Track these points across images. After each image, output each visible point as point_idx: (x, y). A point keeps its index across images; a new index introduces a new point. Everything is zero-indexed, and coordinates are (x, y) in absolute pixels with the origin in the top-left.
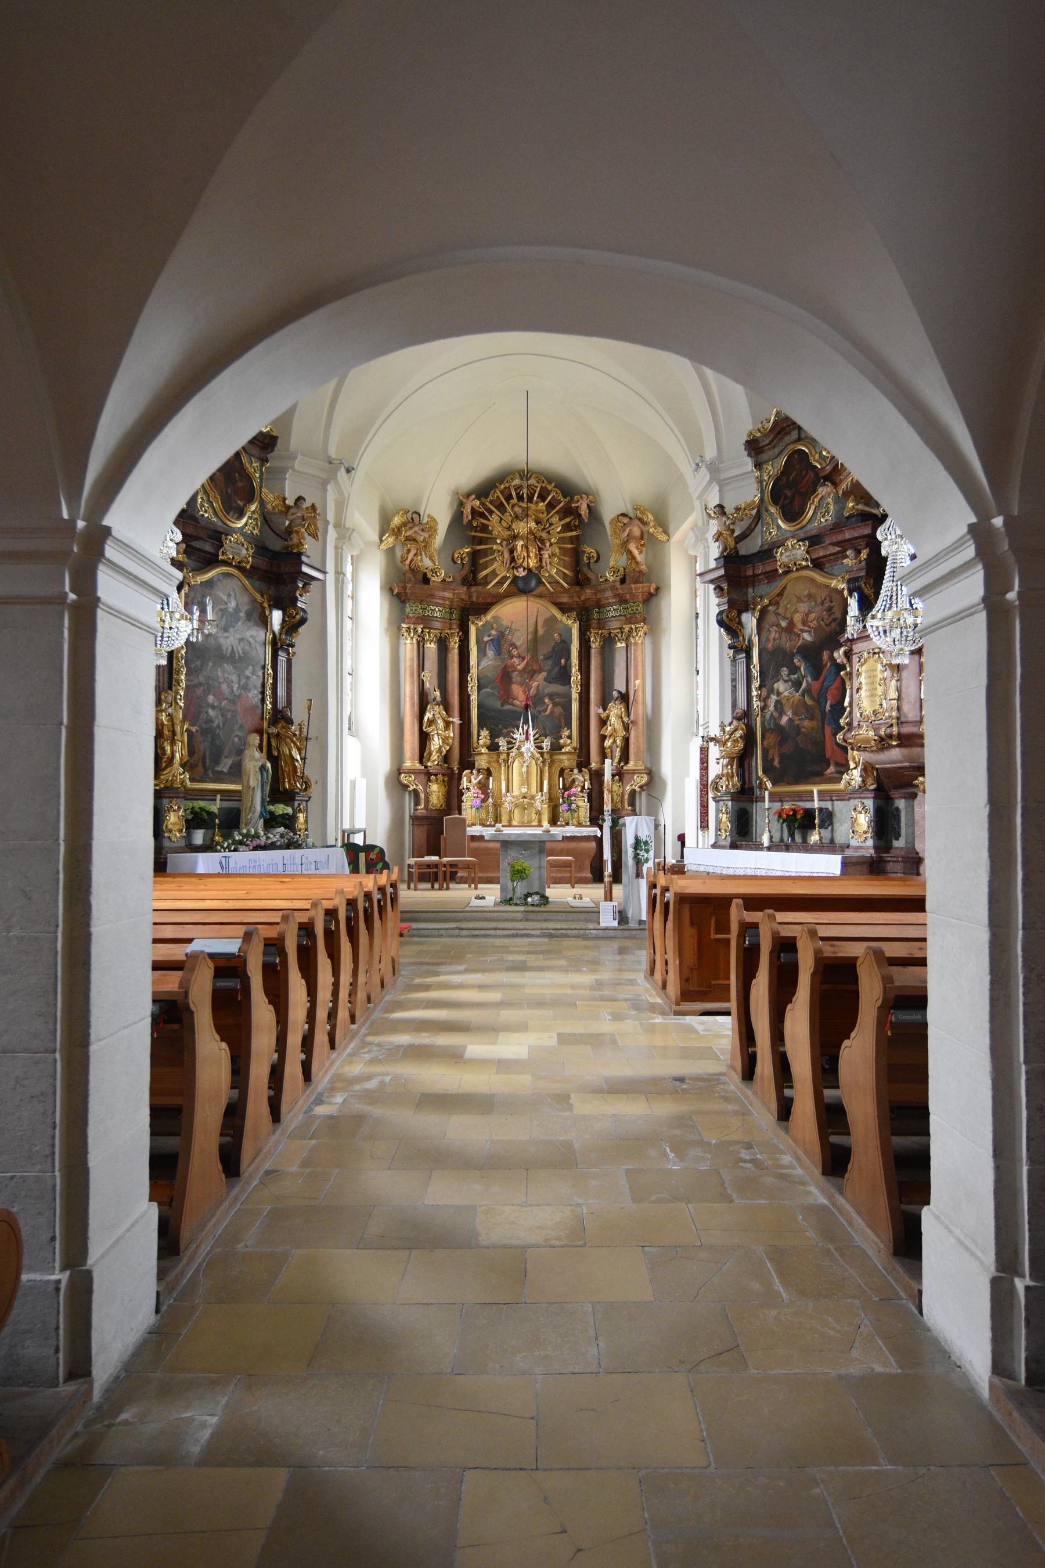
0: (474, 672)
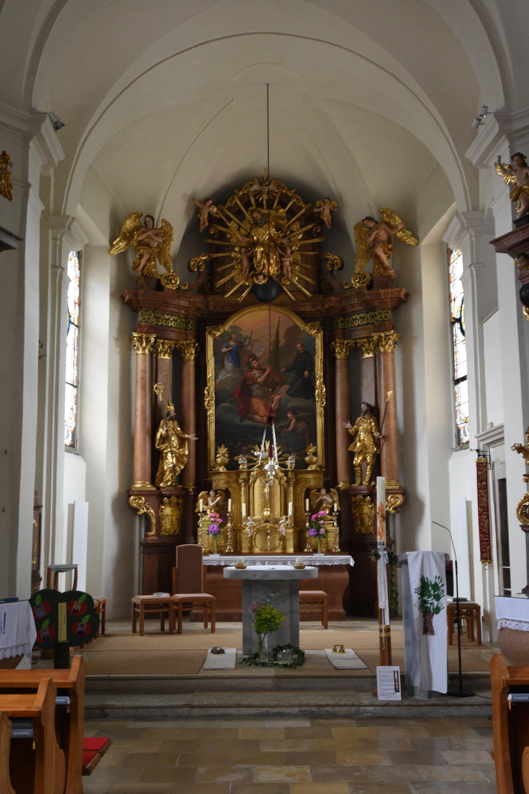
0: (211, 385)
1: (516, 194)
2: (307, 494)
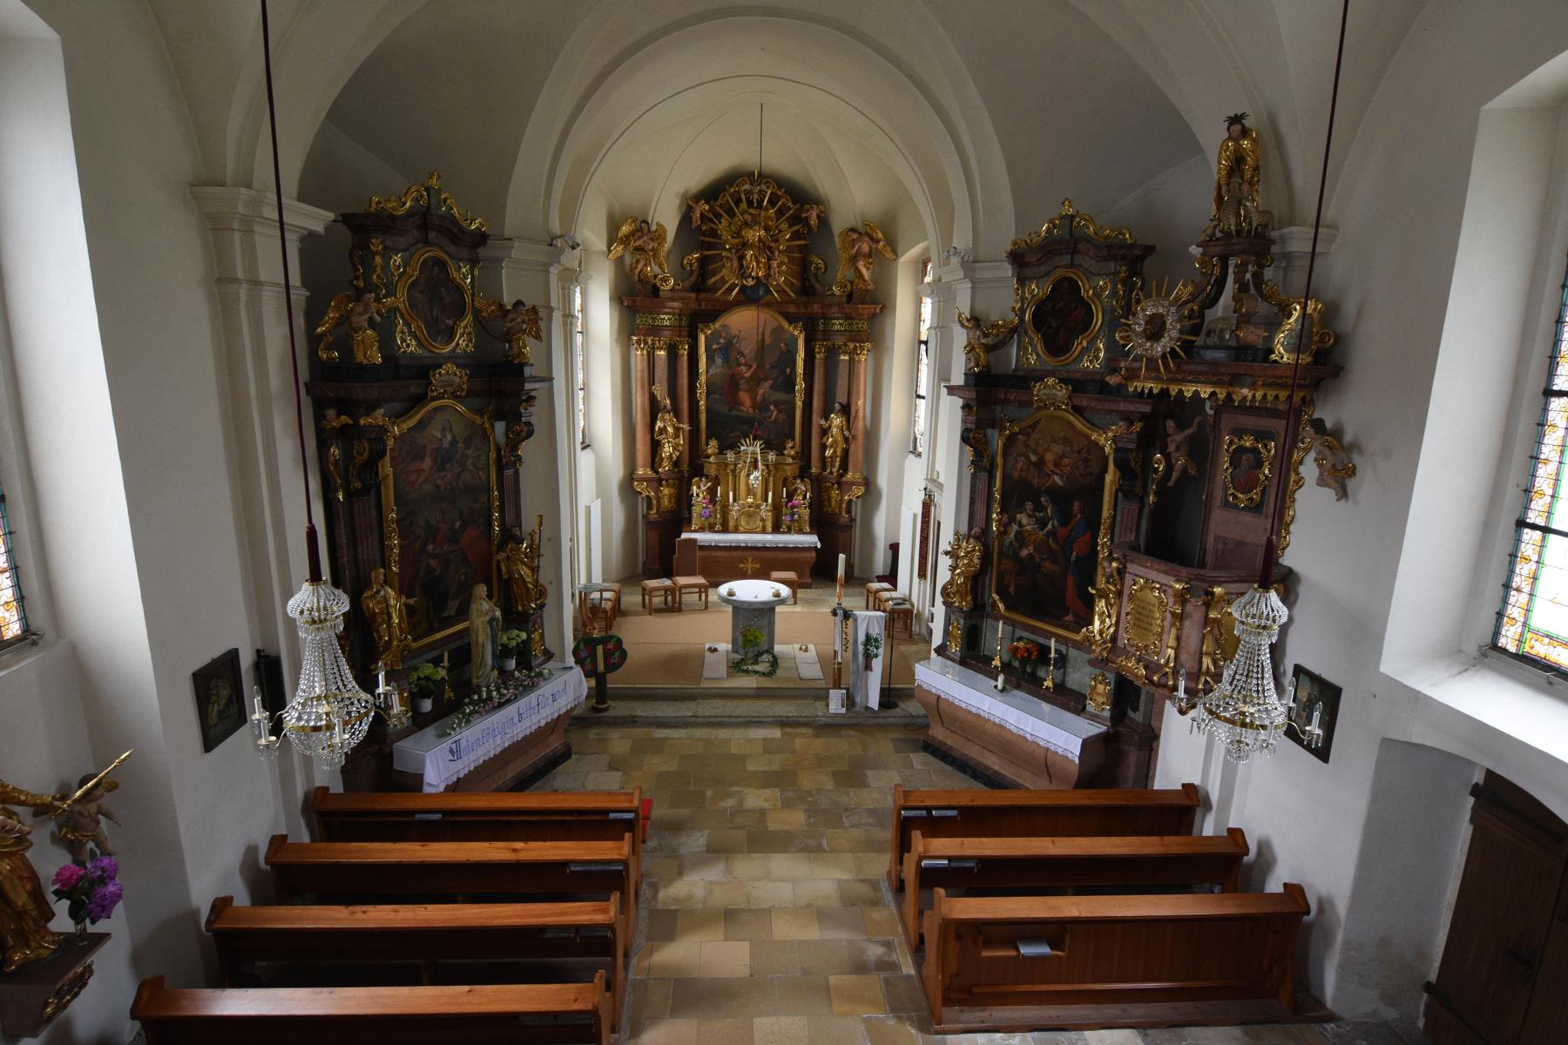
0: (703, 379)
1: (970, 349)
2: (785, 483)
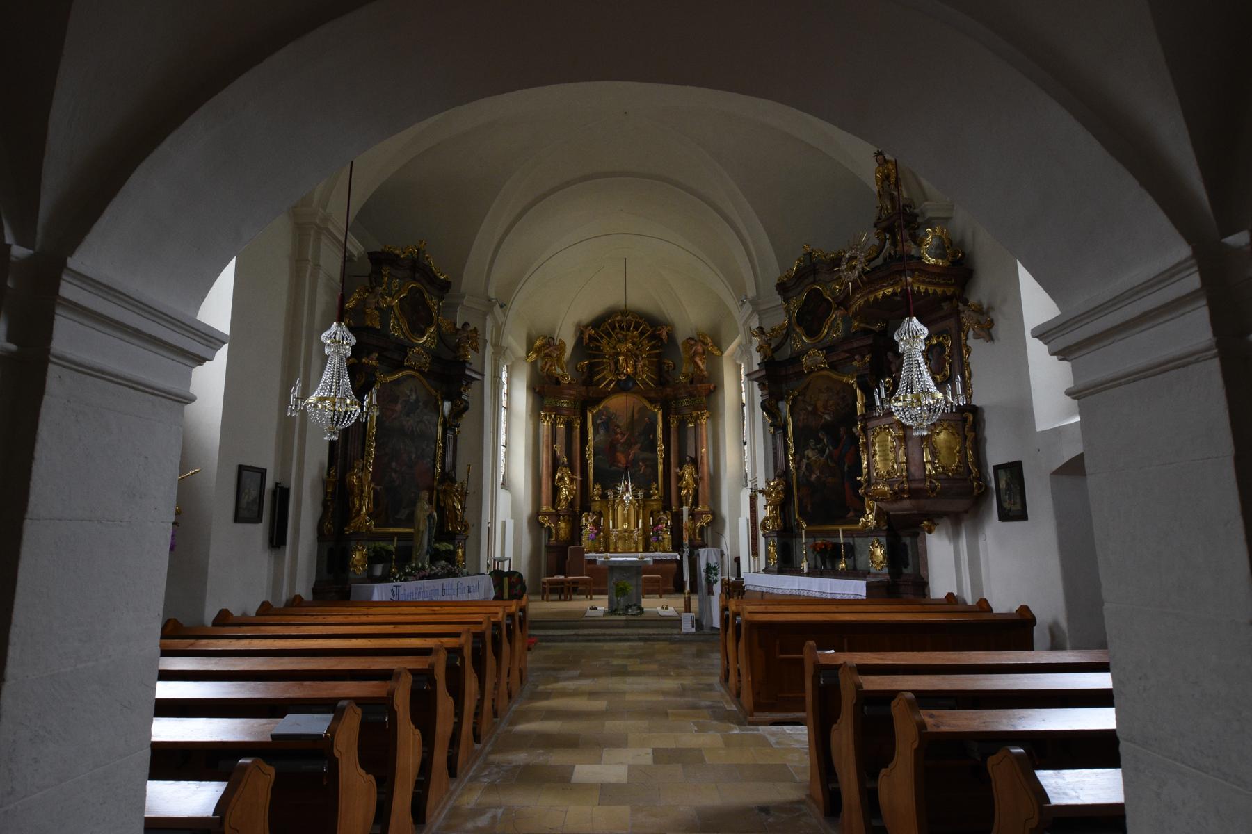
0: (591, 444)
2: (652, 514)
